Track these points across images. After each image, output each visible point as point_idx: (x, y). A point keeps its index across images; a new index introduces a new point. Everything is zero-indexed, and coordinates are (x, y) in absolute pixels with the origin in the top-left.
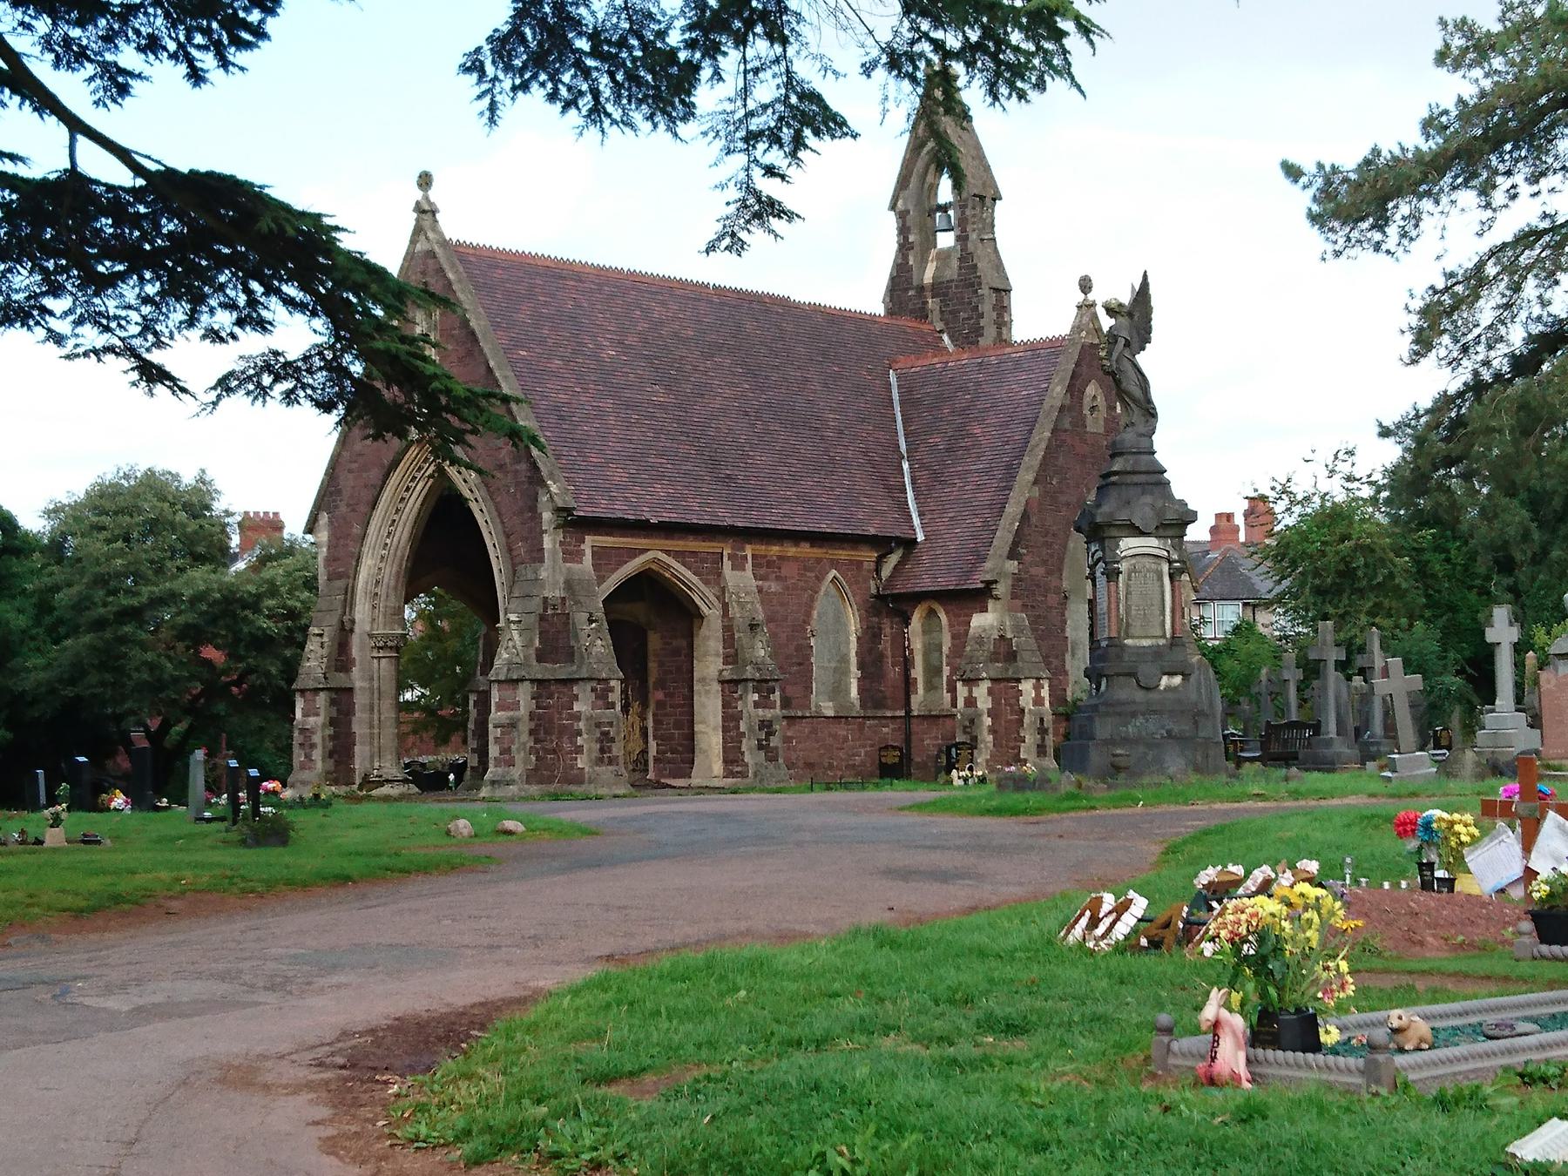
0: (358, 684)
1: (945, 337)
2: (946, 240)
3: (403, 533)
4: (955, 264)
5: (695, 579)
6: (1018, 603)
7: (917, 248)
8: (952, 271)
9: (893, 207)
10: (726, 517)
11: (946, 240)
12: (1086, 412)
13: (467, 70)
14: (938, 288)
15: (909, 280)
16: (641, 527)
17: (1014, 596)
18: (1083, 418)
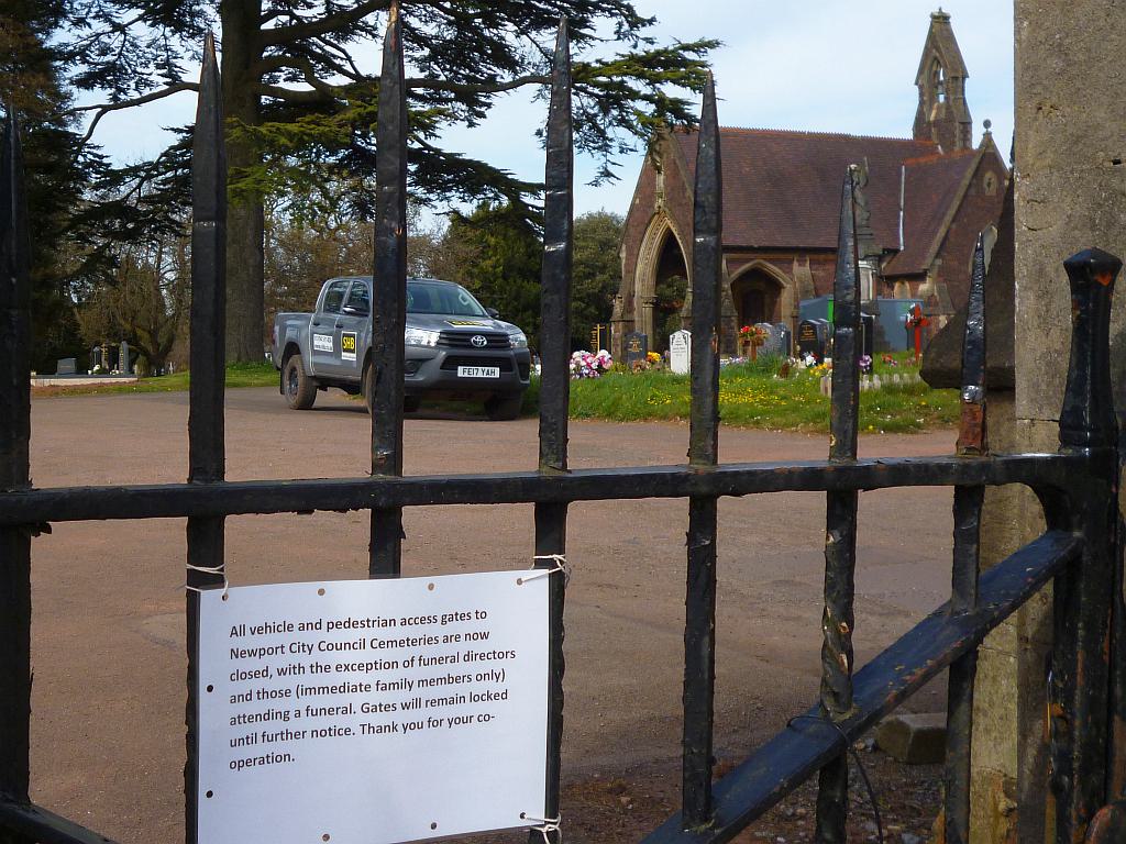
0: (636, 319)
1: (940, 147)
2: (942, 98)
3: (654, 253)
4: (944, 111)
5: (780, 272)
6: (941, 279)
7: (928, 103)
8: (943, 116)
9: (916, 84)
10: (794, 243)
11: (942, 98)
12: (985, 185)
13: (537, 134)
14: (936, 123)
15: (924, 120)
16: (750, 249)
17: (939, 275)
18: (983, 188)
